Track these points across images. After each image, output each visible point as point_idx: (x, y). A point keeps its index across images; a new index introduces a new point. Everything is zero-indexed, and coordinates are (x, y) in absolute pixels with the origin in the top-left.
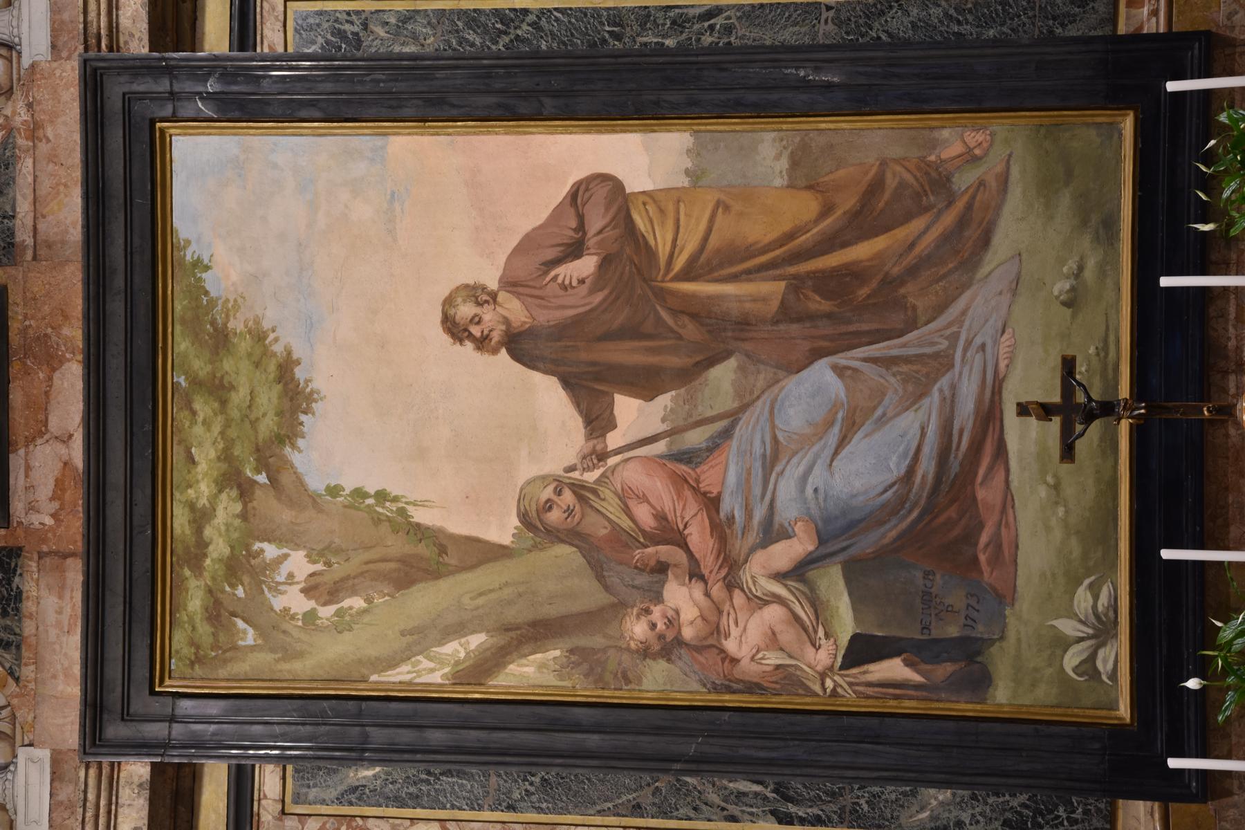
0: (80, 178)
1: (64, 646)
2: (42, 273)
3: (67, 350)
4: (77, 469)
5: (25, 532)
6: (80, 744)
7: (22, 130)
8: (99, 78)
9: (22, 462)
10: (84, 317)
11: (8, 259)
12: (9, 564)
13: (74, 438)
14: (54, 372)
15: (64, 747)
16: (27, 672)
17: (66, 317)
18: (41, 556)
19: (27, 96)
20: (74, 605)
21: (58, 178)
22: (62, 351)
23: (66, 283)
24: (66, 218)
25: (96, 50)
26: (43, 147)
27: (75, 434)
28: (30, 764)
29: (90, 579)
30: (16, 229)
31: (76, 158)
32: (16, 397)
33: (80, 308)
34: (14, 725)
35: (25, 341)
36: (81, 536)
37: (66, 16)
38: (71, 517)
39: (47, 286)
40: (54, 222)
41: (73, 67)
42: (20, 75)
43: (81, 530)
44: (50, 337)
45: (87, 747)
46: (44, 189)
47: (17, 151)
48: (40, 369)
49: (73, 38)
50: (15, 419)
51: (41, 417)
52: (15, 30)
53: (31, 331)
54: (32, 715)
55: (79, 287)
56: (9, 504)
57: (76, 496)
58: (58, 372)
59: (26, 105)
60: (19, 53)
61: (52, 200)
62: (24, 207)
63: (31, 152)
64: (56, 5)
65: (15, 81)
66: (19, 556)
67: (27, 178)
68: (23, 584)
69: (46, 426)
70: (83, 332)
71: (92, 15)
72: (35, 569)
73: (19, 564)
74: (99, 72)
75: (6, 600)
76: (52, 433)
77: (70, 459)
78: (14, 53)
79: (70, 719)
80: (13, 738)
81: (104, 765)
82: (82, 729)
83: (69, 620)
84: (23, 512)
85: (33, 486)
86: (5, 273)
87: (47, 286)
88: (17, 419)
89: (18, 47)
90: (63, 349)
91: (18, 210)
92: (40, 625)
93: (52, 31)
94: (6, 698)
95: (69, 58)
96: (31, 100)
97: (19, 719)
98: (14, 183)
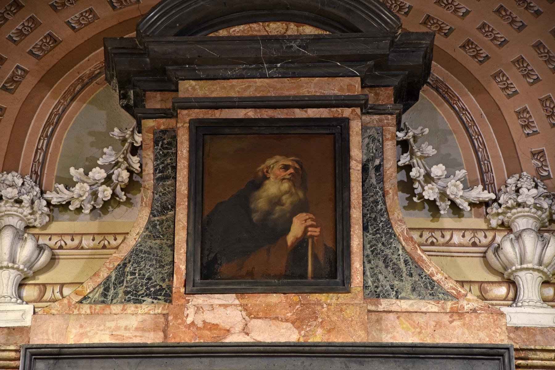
0: (426, 342)
1: (103, 332)
2: (359, 316)
3: (307, 331)
4: (225, 338)
5: (182, 305)
6: (33, 345)
7: (457, 305)
8: (497, 357)
9: (230, 302)
10: (330, 343)
11: (368, 294)
12: (161, 295)
13: (246, 336)
14: (292, 323)
15: (32, 335)
16: (86, 308)
17: (329, 331)
18: (166, 316)
19: (481, 309)
20: (131, 338)
21: (425, 327)
22: (306, 328)
23: (352, 331)
24: (397, 332)
25: (517, 356)
26: (446, 319)
27: (249, 337)
28: (21, 313)
29: (148, 348)
30: (389, 300)
31: (440, 340)
32: (274, 298)
33: (336, 340)
34: (49, 301)
35: (313, 304)
36: (178, 342)
37: (539, 337)
38: (192, 335)
39: (350, 319)
40: (394, 324)
41: (503, 340)
42: (496, 305)
43: (183, 341)
44: (315, 321)
45: (30, 350)
46: (417, 318)
47: (443, 302)
48: (294, 314)
49: (524, 341)
50: (259, 297)
51: (261, 314)
52: (527, 304)
53: (319, 308)
54: (55, 312)
55: (350, 340)
56: (201, 294)
57: (207, 337)
58: (292, 325)
59: (475, 308)
60: (511, 306)
61: (410, 323)
62: (404, 305)
63: (442, 311)
64: (547, 331)
65: (491, 302)
66: (166, 301)
67: (424, 307)
68: (147, 304)
69: (255, 318)
70: (320, 342)
71: (541, 355)
72: (156, 312)
73: (160, 301)
74: (501, 357)
75: (136, 294)
76: (250, 322)
77: (232, 334)
78: (510, 302)
79: (51, 338)
80: (40, 301)
81: (17, 363)
82: (44, 346)
83: (120, 335)
84: (195, 303)
85: (213, 310)
86: (359, 291)
87: (350, 319)
88: (259, 299)
89: (515, 305)
90: (308, 329)
91: (402, 301)
92: (118, 316)
93: (528, 328)
94: (69, 296)
95: (509, 338)
96: (479, 312)
97: (53, 304)
98: (421, 299)
